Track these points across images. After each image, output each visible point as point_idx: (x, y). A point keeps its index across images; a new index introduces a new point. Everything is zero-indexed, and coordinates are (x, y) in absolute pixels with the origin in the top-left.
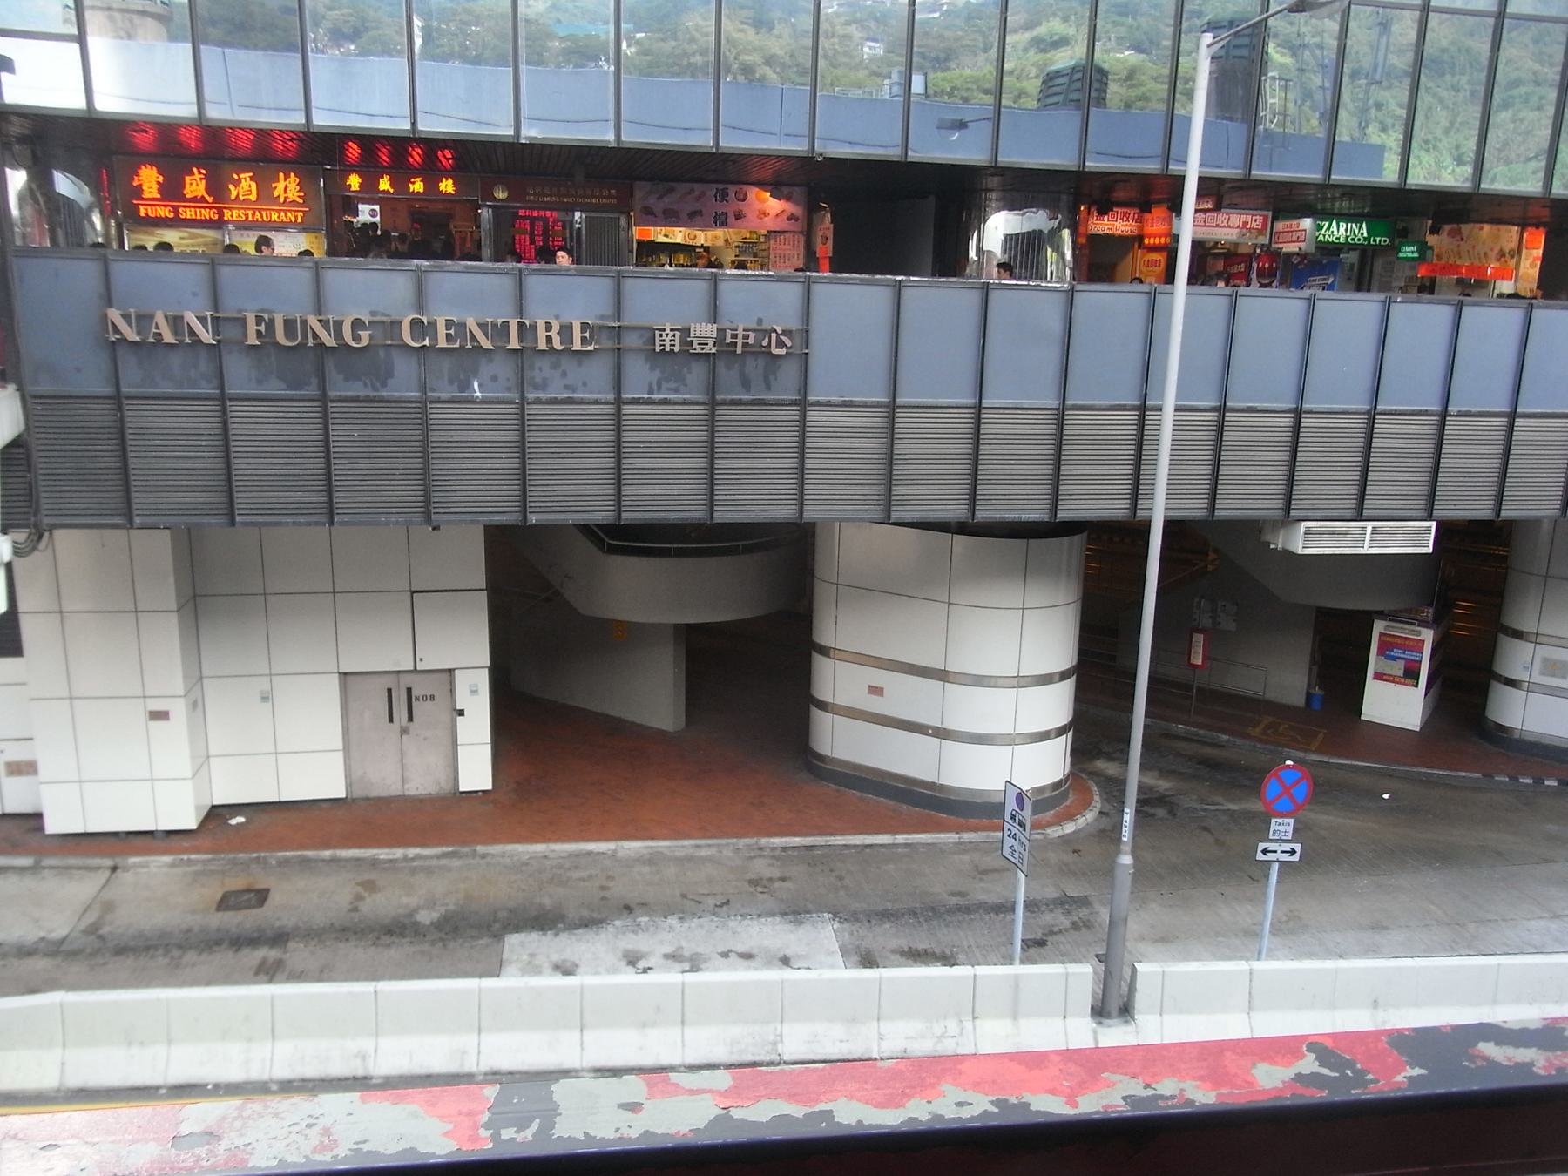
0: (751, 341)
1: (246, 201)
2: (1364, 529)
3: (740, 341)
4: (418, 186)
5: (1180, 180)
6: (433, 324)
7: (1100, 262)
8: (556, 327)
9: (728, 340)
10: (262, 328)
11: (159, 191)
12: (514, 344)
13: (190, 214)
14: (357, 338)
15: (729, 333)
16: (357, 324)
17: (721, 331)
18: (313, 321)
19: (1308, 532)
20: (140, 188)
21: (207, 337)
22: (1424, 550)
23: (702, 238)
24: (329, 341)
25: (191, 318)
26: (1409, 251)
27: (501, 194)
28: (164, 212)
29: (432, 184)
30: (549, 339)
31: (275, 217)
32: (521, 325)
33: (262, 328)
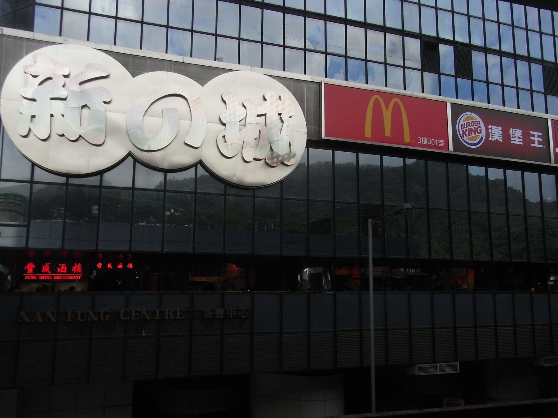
0: (235, 314)
1: (63, 273)
2: (437, 366)
3: (231, 314)
4: (120, 266)
5: (367, 259)
6: (131, 312)
7: (340, 284)
8: (172, 312)
9: (228, 314)
10: (73, 316)
11: (33, 271)
12: (157, 317)
13: (42, 278)
14: (105, 318)
15: (228, 312)
16: (105, 313)
17: (225, 311)
18: (91, 312)
19: (419, 368)
20: (27, 270)
21: (53, 319)
22: (457, 372)
23: (211, 279)
24: (95, 319)
25: (49, 314)
26: (434, 277)
27: (147, 268)
28: (34, 277)
29: (125, 265)
30: (169, 315)
31: (72, 278)
32: (160, 311)
33: (73, 316)
